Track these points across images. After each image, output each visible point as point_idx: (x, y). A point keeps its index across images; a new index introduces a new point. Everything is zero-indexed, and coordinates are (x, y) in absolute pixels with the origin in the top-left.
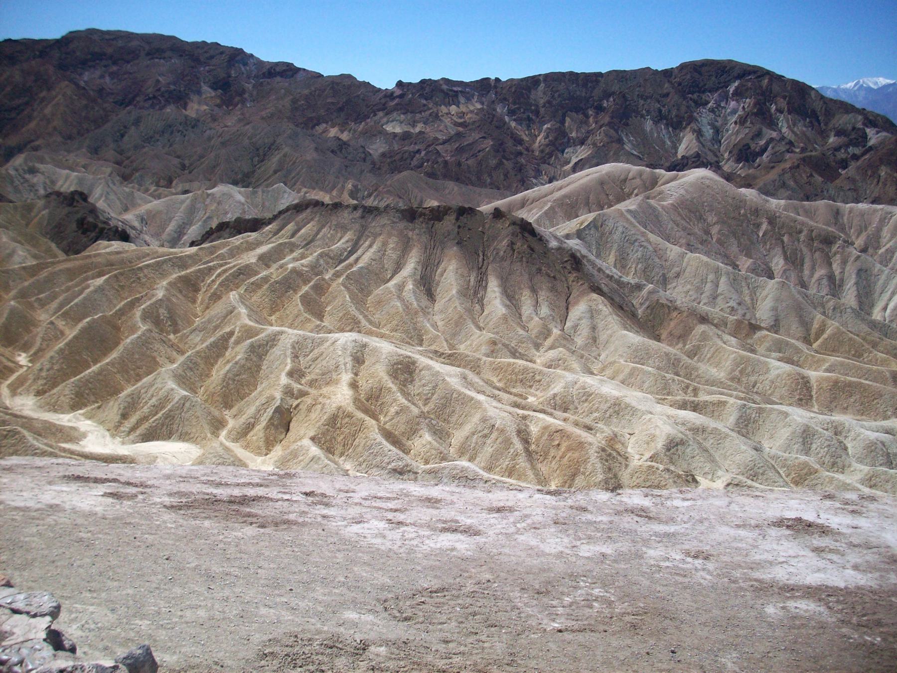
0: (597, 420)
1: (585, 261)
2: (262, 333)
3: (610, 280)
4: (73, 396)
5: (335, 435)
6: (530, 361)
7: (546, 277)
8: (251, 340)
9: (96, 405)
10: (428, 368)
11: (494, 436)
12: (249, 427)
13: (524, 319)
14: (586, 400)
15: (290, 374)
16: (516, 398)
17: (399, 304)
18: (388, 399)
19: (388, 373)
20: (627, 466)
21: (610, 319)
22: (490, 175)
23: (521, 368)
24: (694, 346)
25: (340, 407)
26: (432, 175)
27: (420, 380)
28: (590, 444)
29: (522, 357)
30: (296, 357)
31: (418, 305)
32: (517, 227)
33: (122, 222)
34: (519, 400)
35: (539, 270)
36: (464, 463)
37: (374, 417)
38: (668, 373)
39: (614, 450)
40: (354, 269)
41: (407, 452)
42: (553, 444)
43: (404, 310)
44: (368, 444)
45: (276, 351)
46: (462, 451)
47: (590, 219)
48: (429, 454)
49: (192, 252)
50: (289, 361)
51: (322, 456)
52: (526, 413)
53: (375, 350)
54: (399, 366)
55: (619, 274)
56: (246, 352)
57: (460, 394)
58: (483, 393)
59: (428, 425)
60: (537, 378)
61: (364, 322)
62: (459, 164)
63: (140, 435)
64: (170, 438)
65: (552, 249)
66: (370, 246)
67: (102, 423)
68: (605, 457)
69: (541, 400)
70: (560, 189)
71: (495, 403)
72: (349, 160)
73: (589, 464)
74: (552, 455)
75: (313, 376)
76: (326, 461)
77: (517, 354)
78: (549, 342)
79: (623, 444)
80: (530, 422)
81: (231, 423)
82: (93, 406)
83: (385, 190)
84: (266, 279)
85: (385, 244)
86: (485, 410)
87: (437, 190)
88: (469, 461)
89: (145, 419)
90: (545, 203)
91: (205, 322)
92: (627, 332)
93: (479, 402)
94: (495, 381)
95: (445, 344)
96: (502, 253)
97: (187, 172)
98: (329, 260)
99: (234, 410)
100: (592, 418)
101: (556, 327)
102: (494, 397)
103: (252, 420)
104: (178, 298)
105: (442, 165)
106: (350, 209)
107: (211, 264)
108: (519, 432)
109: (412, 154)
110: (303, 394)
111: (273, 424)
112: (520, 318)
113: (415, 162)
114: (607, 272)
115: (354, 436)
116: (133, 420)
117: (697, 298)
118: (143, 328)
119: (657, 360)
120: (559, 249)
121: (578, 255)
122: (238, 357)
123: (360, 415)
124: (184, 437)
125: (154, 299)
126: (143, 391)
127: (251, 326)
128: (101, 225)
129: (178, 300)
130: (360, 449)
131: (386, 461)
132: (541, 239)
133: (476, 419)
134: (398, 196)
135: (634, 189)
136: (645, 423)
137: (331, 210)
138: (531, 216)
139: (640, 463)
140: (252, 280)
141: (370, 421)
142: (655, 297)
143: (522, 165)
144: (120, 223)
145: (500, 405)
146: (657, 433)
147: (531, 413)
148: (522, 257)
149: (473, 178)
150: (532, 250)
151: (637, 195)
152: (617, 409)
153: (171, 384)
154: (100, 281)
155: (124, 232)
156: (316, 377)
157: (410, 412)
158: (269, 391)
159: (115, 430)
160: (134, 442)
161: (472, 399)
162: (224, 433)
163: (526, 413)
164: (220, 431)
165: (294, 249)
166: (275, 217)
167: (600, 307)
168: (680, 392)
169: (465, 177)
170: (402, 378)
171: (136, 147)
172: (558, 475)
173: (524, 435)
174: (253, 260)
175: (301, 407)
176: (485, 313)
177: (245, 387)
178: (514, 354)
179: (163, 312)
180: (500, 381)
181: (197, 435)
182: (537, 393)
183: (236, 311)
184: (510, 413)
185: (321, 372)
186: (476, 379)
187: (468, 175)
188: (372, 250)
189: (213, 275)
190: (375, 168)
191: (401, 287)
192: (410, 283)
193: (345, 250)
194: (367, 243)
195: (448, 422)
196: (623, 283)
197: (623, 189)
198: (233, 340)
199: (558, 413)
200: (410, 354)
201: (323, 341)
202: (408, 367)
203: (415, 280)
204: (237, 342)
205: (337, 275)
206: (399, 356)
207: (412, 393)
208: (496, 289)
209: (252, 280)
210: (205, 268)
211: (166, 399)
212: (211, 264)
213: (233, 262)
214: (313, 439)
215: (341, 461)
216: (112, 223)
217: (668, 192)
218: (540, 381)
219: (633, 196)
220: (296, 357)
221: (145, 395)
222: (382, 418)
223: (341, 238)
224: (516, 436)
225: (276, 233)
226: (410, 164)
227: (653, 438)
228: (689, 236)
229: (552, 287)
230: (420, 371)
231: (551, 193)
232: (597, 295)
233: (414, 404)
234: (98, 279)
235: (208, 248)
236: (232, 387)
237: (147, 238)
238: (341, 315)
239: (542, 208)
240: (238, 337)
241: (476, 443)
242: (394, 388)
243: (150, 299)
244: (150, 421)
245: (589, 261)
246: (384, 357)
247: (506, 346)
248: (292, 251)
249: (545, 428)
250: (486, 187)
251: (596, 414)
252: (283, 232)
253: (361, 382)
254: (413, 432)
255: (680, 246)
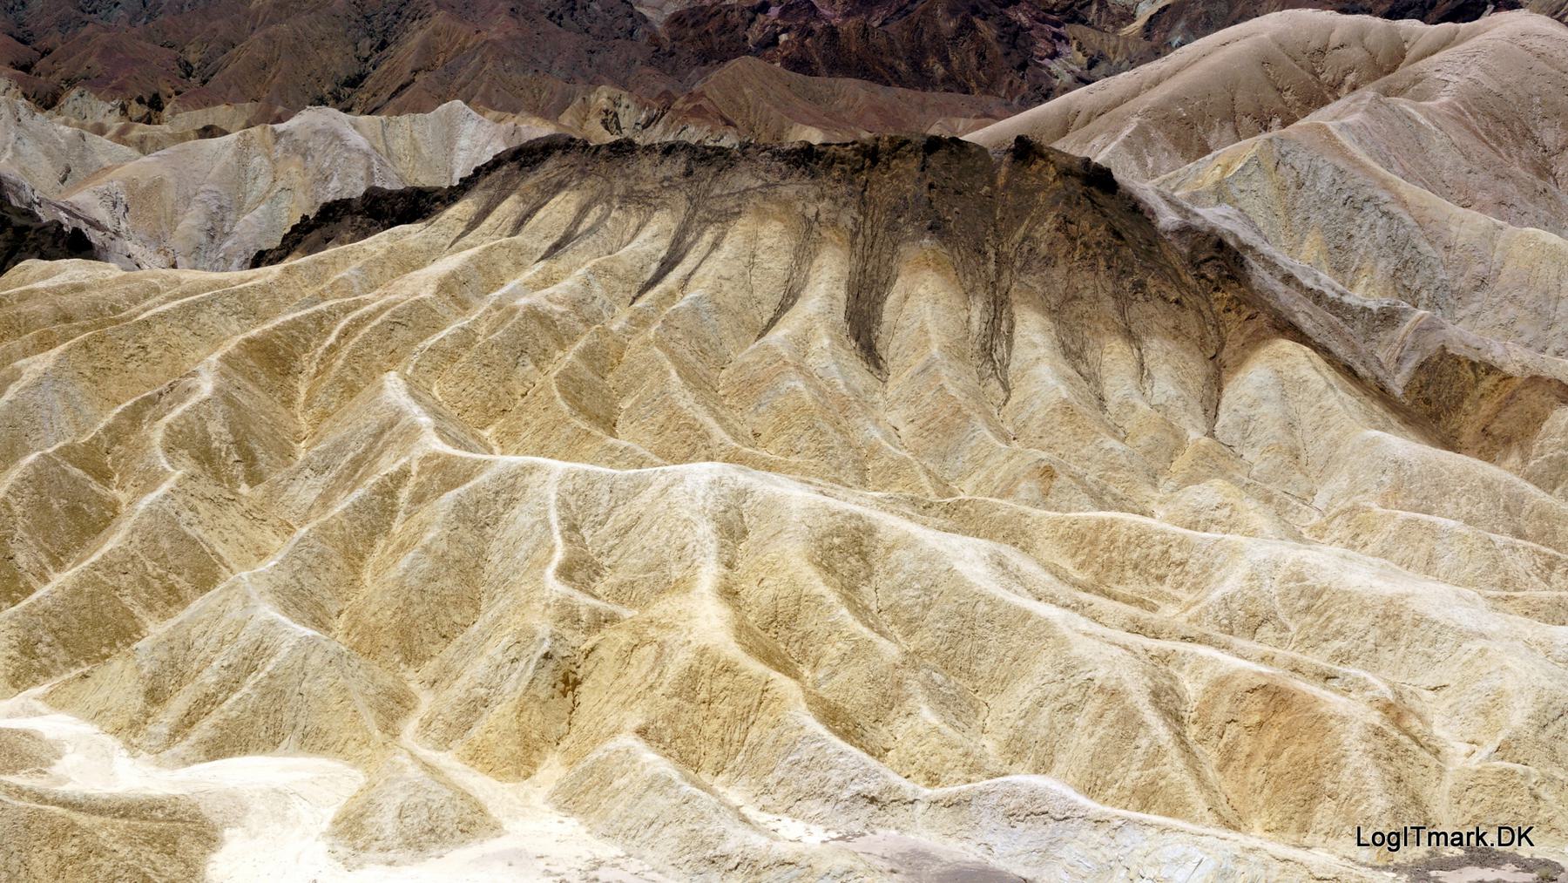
0: (1343, 657)
1: (1248, 257)
2: (481, 471)
3: (1317, 303)
4: (14, 653)
5: (697, 720)
6: (1143, 514)
7: (1159, 303)
8: (455, 491)
9: (75, 672)
10: (910, 543)
11: (1092, 707)
12: (476, 706)
13: (1111, 406)
14: (1308, 609)
15: (566, 572)
16: (1134, 610)
17: (801, 386)
18: (811, 622)
19: (810, 559)
20: (1441, 770)
21: (1331, 400)
22: (946, 61)
23: (1133, 533)
24: (1550, 460)
25: (705, 649)
26: (800, 64)
27: (890, 574)
28: (1344, 720)
29: (1120, 504)
30: (574, 528)
31: (846, 384)
32: (1076, 182)
33: (68, 212)
34: (1145, 615)
35: (1140, 286)
36: (1024, 779)
37: (787, 669)
38: (1497, 532)
39: (1406, 732)
40: (682, 303)
41: (879, 753)
42: (1248, 723)
43: (815, 399)
44: (784, 740)
45: (521, 517)
46: (1016, 750)
47: (1251, 153)
48: (936, 759)
49: (270, 278)
50: (558, 540)
51: (675, 775)
52: (1166, 645)
53: (771, 504)
54: (837, 541)
55: (1340, 287)
56: (446, 522)
57: (992, 602)
58: (1052, 600)
59: (924, 685)
60: (1177, 555)
61: (718, 433)
62: (866, 32)
63: (200, 742)
64: (276, 745)
65: (1166, 233)
66: (715, 245)
67: (97, 716)
68: (1384, 752)
69: (1194, 610)
70: (1157, 82)
71: (1084, 624)
72: (597, 37)
73: (1347, 772)
74: (1247, 750)
75: (621, 576)
76: (687, 788)
77: (1108, 499)
78: (1182, 462)
79: (1420, 717)
80: (1180, 669)
81: (426, 702)
82: (66, 676)
83: (690, 106)
84: (466, 338)
85: (753, 238)
86: (1063, 643)
87: (815, 100)
88: (1036, 772)
89: (208, 701)
90: (1124, 120)
91: (326, 451)
92: (1377, 433)
93: (1046, 623)
94: (1070, 569)
95: (924, 479)
96: (1043, 248)
97: (196, 81)
98: (614, 283)
99: (430, 668)
100: (1330, 652)
101: (1194, 426)
102: (1078, 607)
103: (482, 691)
104: (252, 396)
105: (824, 39)
106: (657, 156)
107: (323, 306)
108: (1156, 695)
109: (748, 15)
110: (601, 621)
111: (535, 698)
112: (1103, 408)
113: (754, 35)
114: (1308, 282)
115: (745, 718)
116: (179, 704)
117: (1537, 338)
118: (176, 473)
119: (1463, 501)
120: (1184, 231)
121: (1232, 243)
122: (429, 536)
123: (757, 668)
124: (313, 741)
125: (193, 400)
126: (195, 632)
127: (449, 457)
128: (17, 221)
129: (253, 398)
130: (764, 753)
131: (834, 779)
132: (1136, 210)
133: (1043, 667)
134: (722, 117)
135: (1346, 73)
136: (1471, 662)
137: (607, 159)
138: (1102, 153)
139: (1474, 763)
140: (430, 342)
141: (782, 682)
142: (1432, 344)
143: (1021, 28)
144: (62, 214)
145: (1097, 628)
146: (1510, 684)
147: (1182, 647)
148: (1095, 256)
149: (903, 67)
150: (1118, 235)
151: (1354, 88)
152: (1391, 627)
153: (267, 611)
154: (44, 361)
155: (77, 232)
156: (629, 577)
157: (878, 654)
158: (518, 618)
159: (131, 730)
160: (185, 762)
161: (1027, 616)
162: (409, 728)
163: (1166, 645)
164: (400, 723)
165: (524, 260)
166: (466, 185)
167: (1303, 373)
168: (1535, 579)
169: (883, 65)
170: (843, 568)
171: (63, 25)
172: (1267, 801)
173: (1166, 699)
174: (427, 293)
175: (601, 652)
176: (1013, 401)
177: (451, 610)
178: (1099, 498)
179: (217, 429)
180: (1081, 566)
181: (346, 735)
182: (1178, 594)
183: (404, 421)
184: (1126, 648)
185: (641, 563)
186: (1028, 566)
187: (888, 60)
188: (720, 255)
189: (329, 333)
190: (661, 56)
191: (802, 343)
192: (822, 331)
193: (650, 256)
194: (708, 237)
195: (972, 676)
196: (1349, 309)
197: (1316, 75)
198: (404, 494)
199: (1240, 642)
200: (858, 509)
201: (638, 487)
202: (857, 542)
203: (833, 326)
204: (419, 498)
205: (641, 321)
206: (833, 515)
207: (873, 606)
208: (1038, 338)
209: (430, 342)
210: (308, 317)
211: (259, 651)
212: (323, 306)
213: (374, 300)
214: (642, 732)
215: (718, 783)
216: (45, 215)
217: (1438, 75)
218: (1182, 564)
219: (1345, 89)
220: (574, 528)
221: (202, 641)
222: (806, 671)
223: (639, 229)
224: (1148, 706)
225: (472, 225)
226: (746, 39)
227: (1496, 701)
228: (1500, 184)
229: (1176, 328)
230: (889, 549)
231: (1136, 93)
232: (1290, 343)
233: (882, 633)
234: (40, 356)
235: (307, 267)
236: (419, 610)
237: (133, 248)
238: (661, 418)
239: (1117, 131)
240: (421, 485)
241: (1052, 728)
242: (832, 597)
243: (182, 401)
244: (224, 707)
245: (1259, 256)
246: (795, 517)
247: (1078, 479)
248: (519, 266)
249: (1222, 683)
250: (934, 86)
251: (1337, 644)
252: (490, 220)
253: (748, 588)
254: (889, 701)
255: (1480, 210)
